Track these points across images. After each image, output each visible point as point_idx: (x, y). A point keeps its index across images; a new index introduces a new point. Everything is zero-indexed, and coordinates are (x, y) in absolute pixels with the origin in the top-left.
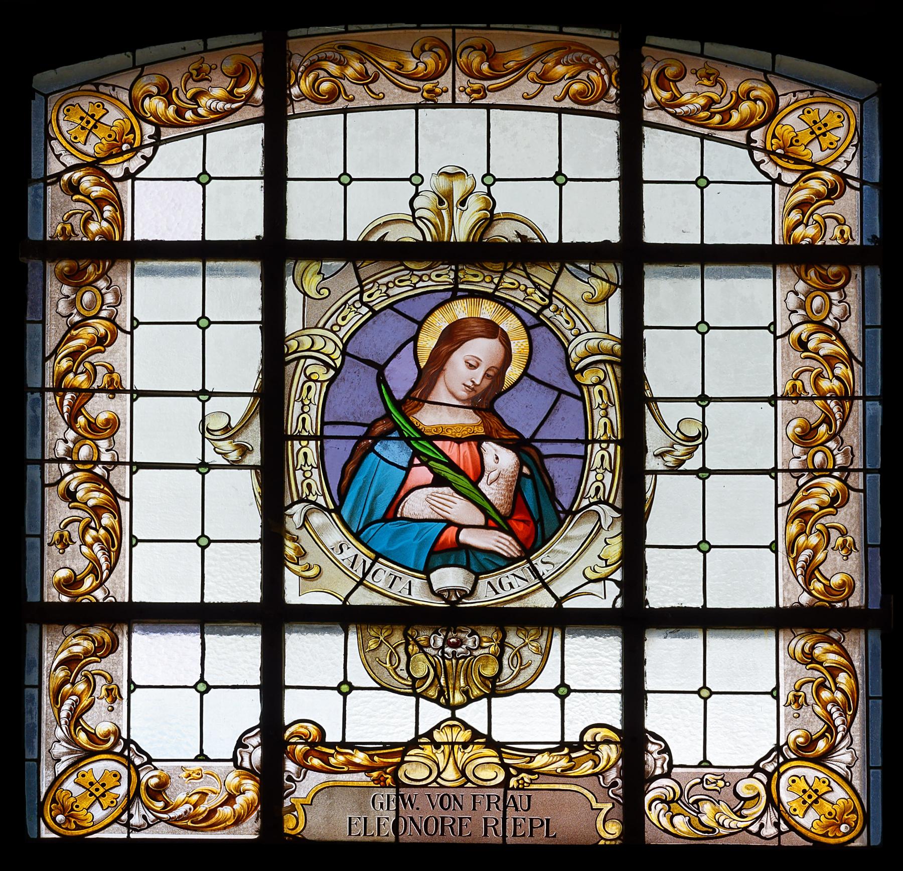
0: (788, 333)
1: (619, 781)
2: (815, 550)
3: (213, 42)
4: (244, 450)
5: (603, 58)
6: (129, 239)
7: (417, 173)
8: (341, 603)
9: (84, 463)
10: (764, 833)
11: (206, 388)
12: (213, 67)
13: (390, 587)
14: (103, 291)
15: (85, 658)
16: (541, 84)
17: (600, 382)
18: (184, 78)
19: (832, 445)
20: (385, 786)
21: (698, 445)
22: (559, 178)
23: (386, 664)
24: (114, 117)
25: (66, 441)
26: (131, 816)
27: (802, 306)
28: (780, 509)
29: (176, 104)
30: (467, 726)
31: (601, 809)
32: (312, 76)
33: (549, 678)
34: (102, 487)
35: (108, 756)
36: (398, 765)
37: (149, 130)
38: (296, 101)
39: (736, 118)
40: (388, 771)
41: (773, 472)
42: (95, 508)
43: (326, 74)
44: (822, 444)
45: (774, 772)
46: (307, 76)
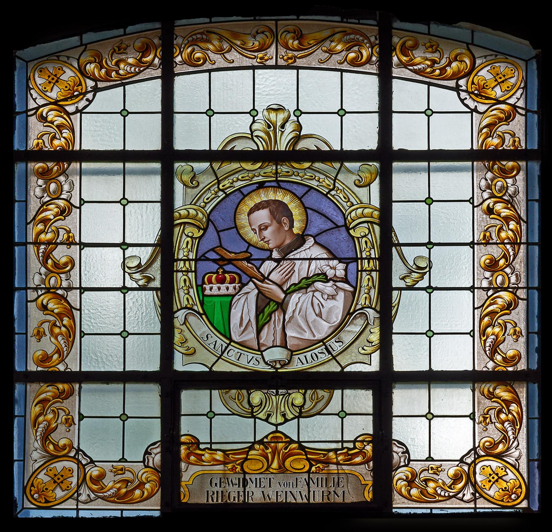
0: (481, 204)
3: (130, 29)
4: (150, 280)
5: (368, 37)
6: (78, 148)
7: (254, 109)
8: (209, 370)
10: (465, 498)
11: (126, 285)
12: (129, 45)
15: (53, 399)
17: (365, 236)
19: (508, 270)
20: (236, 473)
21: (426, 273)
22: (342, 113)
24: (68, 75)
25: (40, 274)
26: (79, 495)
27: (489, 187)
28: (476, 311)
29: (105, 68)
31: (368, 484)
32: (190, 49)
34: (63, 114)
35: (67, 459)
38: (178, 64)
39: (449, 71)
40: (237, 463)
42: (58, 127)
43: (199, 49)
45: (472, 463)
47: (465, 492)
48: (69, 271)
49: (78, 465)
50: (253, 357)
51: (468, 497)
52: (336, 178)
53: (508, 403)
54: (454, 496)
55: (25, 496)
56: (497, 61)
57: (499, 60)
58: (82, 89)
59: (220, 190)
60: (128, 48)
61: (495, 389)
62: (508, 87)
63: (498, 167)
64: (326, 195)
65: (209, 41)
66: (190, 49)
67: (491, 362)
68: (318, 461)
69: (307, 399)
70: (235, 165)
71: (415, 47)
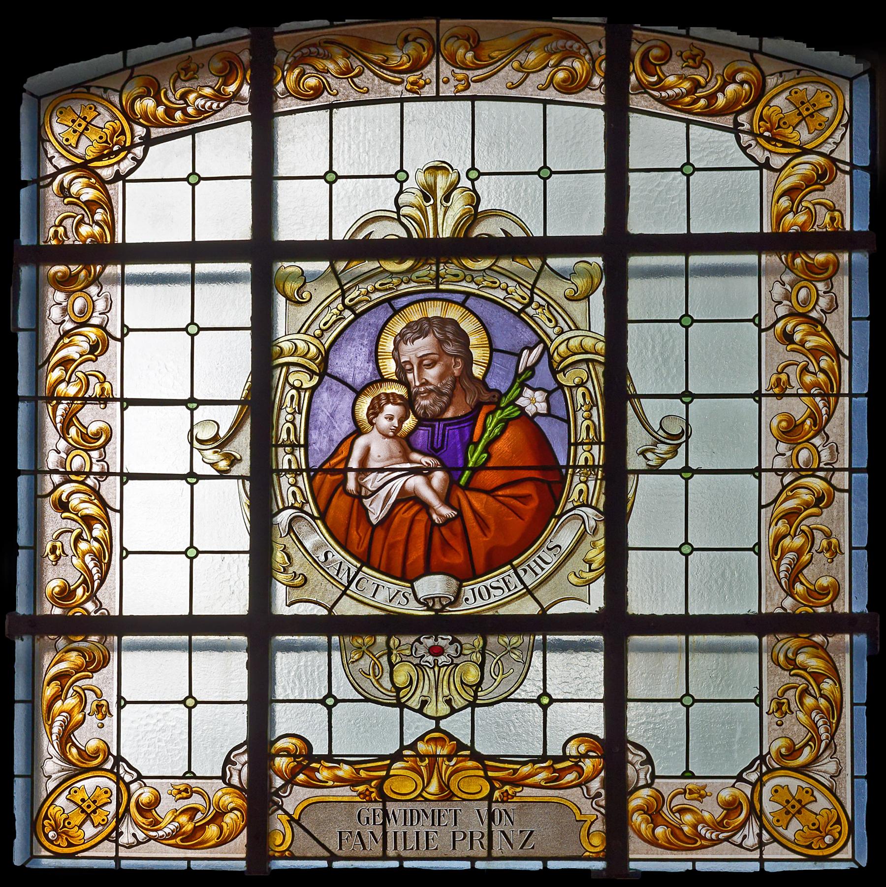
0: (773, 325)
1: (603, 791)
2: (799, 552)
7: (402, 170)
9: (78, 473)
11: (195, 396)
12: (201, 66)
13: (373, 596)
14: (94, 299)
16: (526, 72)
17: (582, 384)
18: (173, 77)
20: (370, 801)
23: (369, 675)
25: (59, 452)
26: (120, 834)
27: (787, 297)
28: (763, 511)
29: (165, 105)
30: (452, 738)
31: (586, 821)
32: (297, 71)
33: (531, 689)
36: (383, 779)
37: (140, 131)
39: (721, 101)
40: (373, 784)
41: (757, 472)
44: (807, 441)
46: (292, 71)
47: (746, 832)
48: (103, 446)
49: (117, 783)
50: (398, 591)
51: (751, 841)
52: (534, 286)
53: (818, 677)
54: (727, 839)
55: (34, 837)
56: (800, 81)
57: (805, 80)
58: (125, 142)
59: (346, 307)
60: (200, 70)
61: (797, 654)
62: (820, 125)
63: (802, 263)
64: (517, 314)
65: (330, 57)
66: (297, 71)
67: (790, 599)
68: (504, 782)
69: (486, 674)
70: (369, 266)
71: (666, 58)
